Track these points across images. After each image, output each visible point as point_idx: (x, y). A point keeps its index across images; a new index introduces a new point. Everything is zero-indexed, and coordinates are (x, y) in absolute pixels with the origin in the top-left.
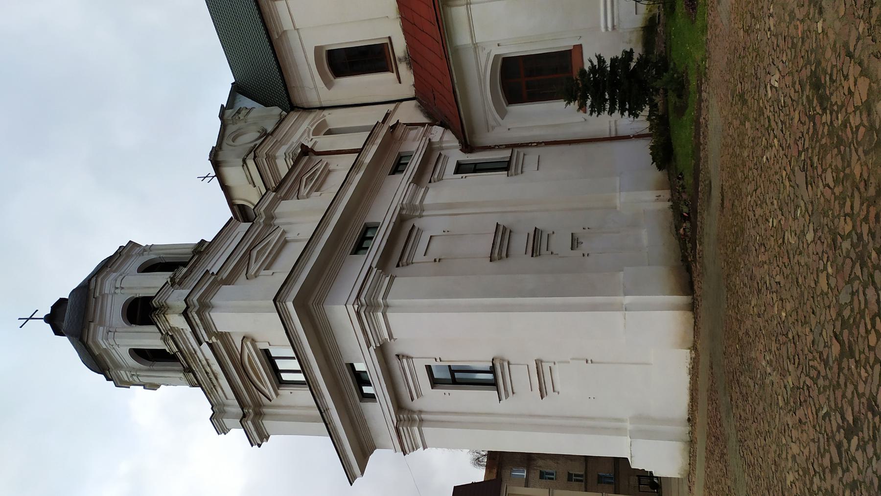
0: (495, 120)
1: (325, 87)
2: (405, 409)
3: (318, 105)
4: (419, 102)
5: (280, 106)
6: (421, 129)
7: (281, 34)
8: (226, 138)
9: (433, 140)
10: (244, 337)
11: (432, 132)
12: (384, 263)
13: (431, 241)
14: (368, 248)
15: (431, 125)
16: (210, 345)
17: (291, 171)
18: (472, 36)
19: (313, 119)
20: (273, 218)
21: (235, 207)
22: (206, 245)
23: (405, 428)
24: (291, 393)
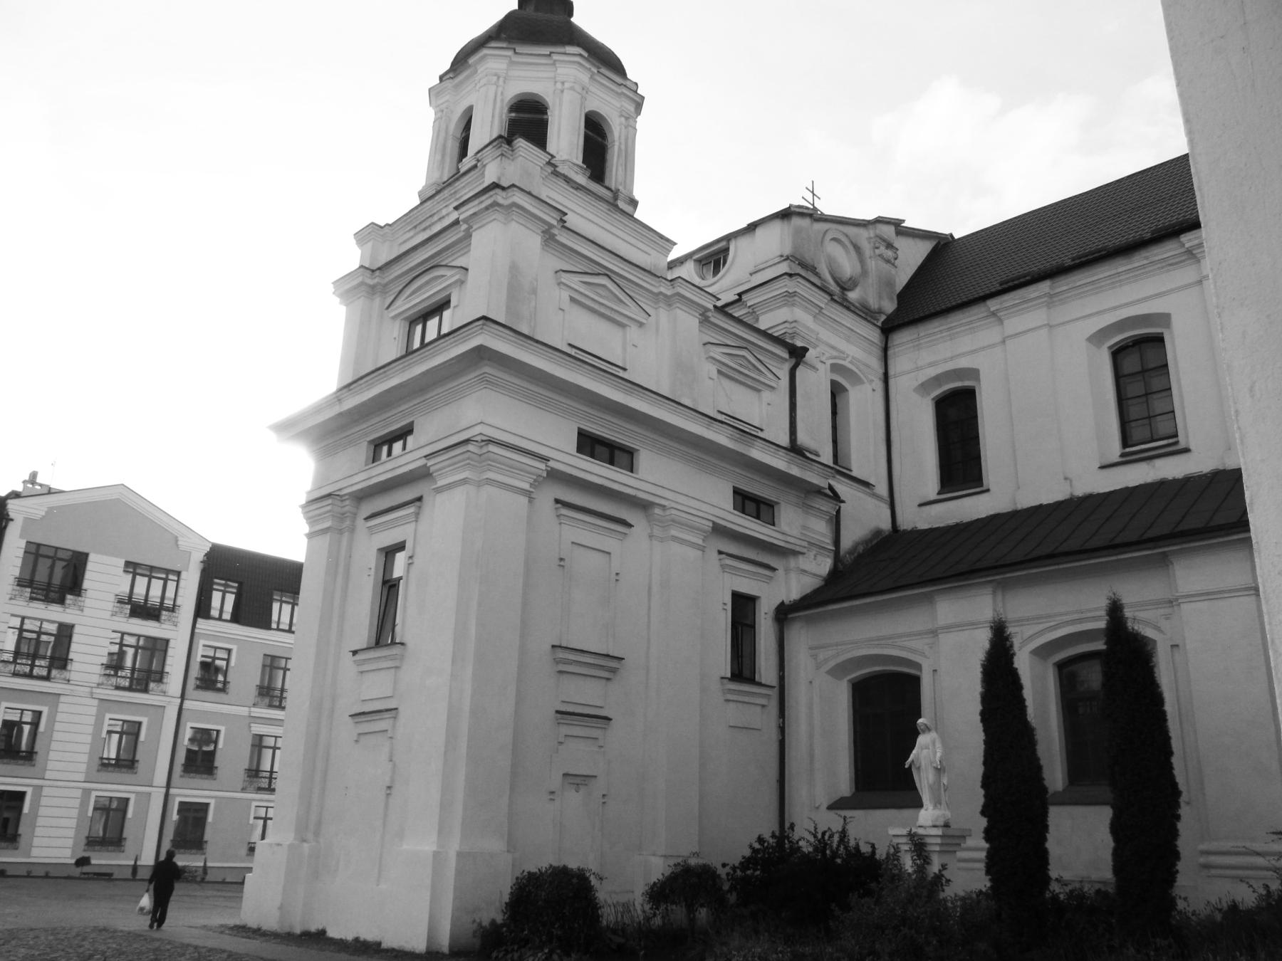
2: (357, 508)
3: (891, 372)
5: (897, 310)
6: (828, 541)
12: (555, 476)
13: (601, 554)
16: (456, 222)
17: (764, 334)
22: (628, 208)
23: (329, 508)
24: (395, 338)
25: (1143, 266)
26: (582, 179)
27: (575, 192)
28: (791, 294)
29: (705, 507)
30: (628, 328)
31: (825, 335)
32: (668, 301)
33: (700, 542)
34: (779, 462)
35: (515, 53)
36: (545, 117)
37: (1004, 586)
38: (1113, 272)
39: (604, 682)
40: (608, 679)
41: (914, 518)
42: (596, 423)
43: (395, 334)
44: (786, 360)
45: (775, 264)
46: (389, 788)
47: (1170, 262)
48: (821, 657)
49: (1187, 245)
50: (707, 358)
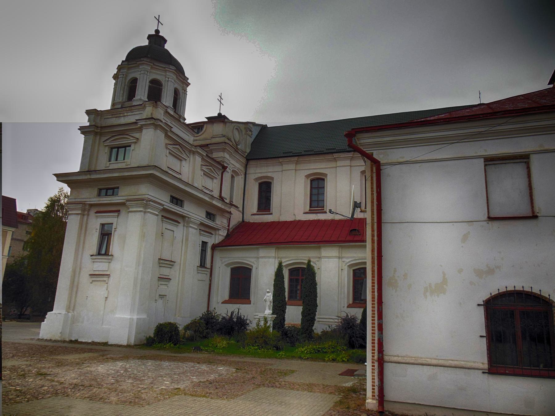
0: (225, 262)
1: (255, 178)
3: (247, 172)
5: (250, 152)
9: (220, 231)
10: (138, 139)
11: (224, 230)
12: (165, 210)
15: (228, 230)
17: (213, 159)
18: (262, 257)
19: (241, 170)
20: (194, 154)
23: (81, 207)
24: (106, 153)
25: (323, 159)
26: (172, 113)
27: (170, 117)
29: (199, 218)
31: (233, 162)
32: (194, 153)
34: (219, 204)
35: (154, 64)
36: (161, 87)
37: (278, 248)
38: (315, 159)
40: (171, 268)
41: (250, 219)
43: (106, 151)
45: (220, 137)
46: (106, 298)
48: (223, 261)
49: (335, 157)
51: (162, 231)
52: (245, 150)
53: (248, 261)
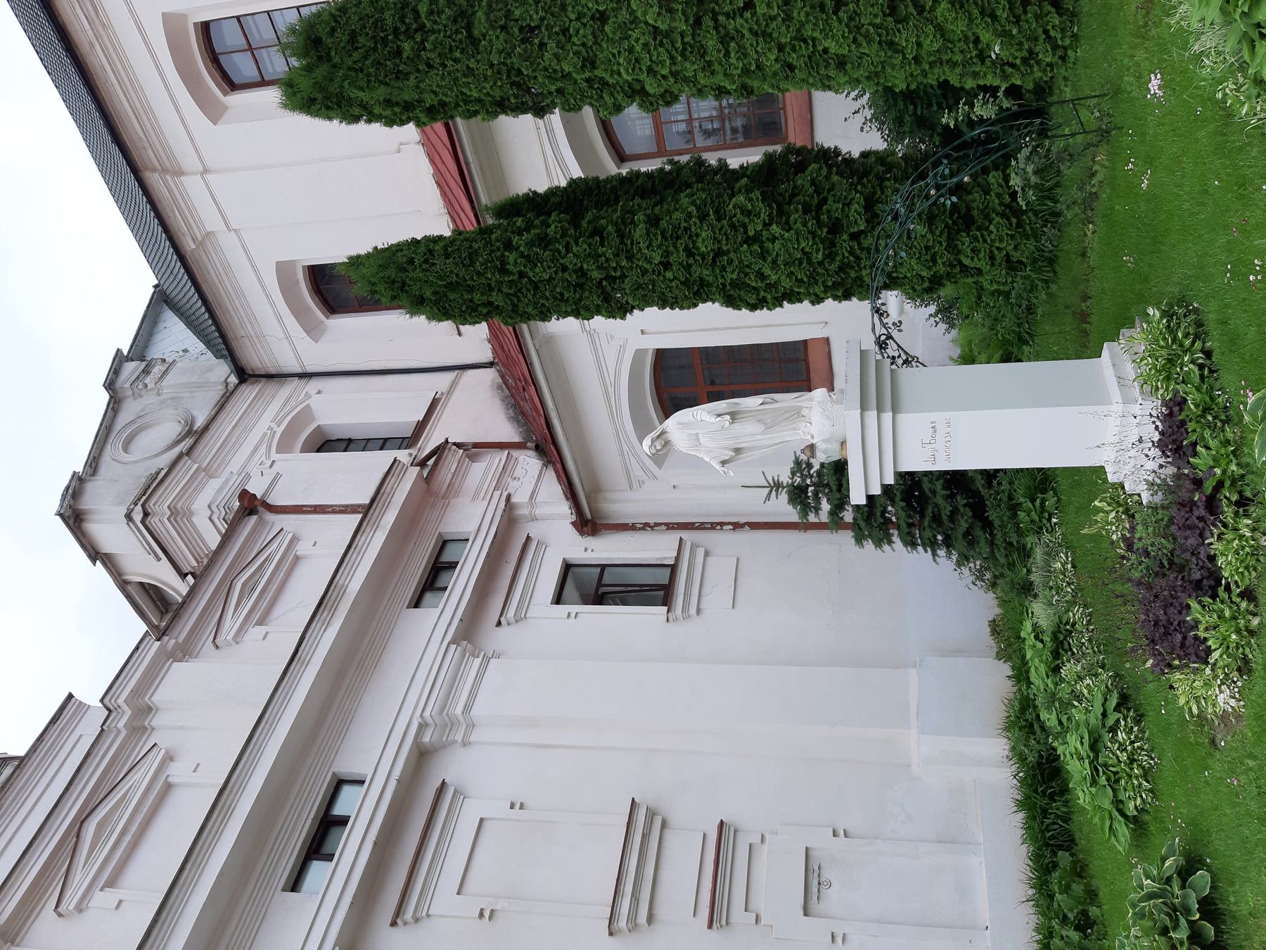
3: (298, 369)
4: (502, 377)
7: (203, 238)
8: (113, 435)
14: (445, 589)
19: (285, 405)
21: (129, 588)
28: (172, 514)
30: (170, 780)
31: (235, 464)
33: (478, 661)
39: (669, 834)
42: (279, 859)
44: (260, 518)
47: (92, 13)
50: (237, 643)
51: (474, 918)
52: (220, 388)
53: (617, 375)
